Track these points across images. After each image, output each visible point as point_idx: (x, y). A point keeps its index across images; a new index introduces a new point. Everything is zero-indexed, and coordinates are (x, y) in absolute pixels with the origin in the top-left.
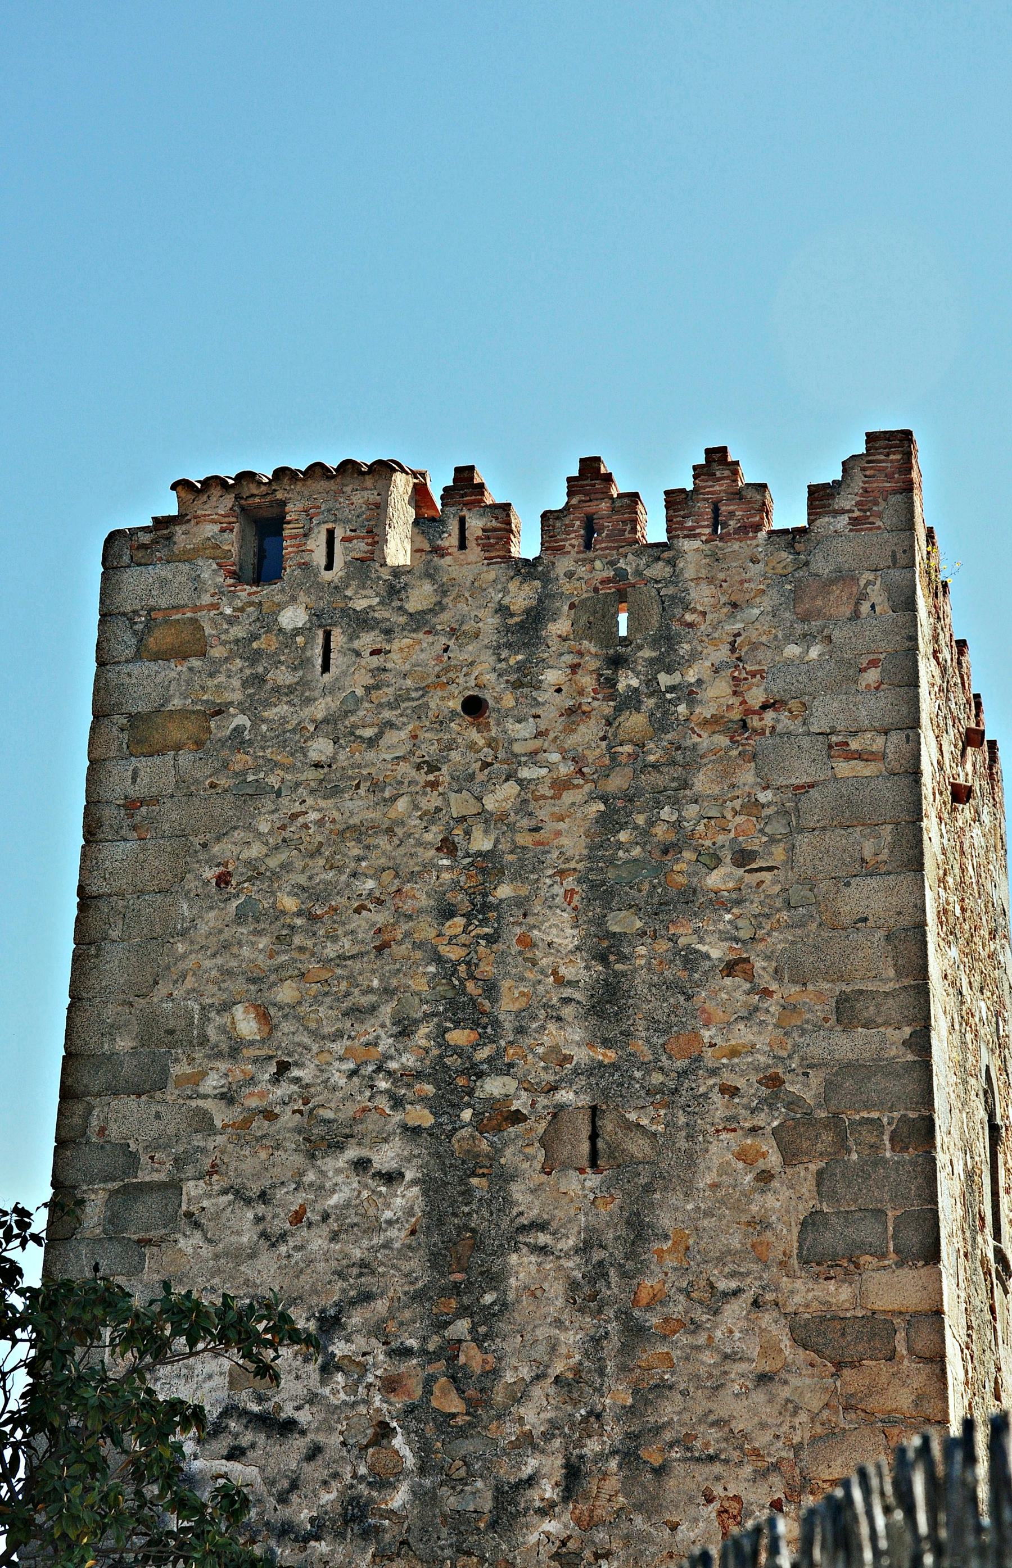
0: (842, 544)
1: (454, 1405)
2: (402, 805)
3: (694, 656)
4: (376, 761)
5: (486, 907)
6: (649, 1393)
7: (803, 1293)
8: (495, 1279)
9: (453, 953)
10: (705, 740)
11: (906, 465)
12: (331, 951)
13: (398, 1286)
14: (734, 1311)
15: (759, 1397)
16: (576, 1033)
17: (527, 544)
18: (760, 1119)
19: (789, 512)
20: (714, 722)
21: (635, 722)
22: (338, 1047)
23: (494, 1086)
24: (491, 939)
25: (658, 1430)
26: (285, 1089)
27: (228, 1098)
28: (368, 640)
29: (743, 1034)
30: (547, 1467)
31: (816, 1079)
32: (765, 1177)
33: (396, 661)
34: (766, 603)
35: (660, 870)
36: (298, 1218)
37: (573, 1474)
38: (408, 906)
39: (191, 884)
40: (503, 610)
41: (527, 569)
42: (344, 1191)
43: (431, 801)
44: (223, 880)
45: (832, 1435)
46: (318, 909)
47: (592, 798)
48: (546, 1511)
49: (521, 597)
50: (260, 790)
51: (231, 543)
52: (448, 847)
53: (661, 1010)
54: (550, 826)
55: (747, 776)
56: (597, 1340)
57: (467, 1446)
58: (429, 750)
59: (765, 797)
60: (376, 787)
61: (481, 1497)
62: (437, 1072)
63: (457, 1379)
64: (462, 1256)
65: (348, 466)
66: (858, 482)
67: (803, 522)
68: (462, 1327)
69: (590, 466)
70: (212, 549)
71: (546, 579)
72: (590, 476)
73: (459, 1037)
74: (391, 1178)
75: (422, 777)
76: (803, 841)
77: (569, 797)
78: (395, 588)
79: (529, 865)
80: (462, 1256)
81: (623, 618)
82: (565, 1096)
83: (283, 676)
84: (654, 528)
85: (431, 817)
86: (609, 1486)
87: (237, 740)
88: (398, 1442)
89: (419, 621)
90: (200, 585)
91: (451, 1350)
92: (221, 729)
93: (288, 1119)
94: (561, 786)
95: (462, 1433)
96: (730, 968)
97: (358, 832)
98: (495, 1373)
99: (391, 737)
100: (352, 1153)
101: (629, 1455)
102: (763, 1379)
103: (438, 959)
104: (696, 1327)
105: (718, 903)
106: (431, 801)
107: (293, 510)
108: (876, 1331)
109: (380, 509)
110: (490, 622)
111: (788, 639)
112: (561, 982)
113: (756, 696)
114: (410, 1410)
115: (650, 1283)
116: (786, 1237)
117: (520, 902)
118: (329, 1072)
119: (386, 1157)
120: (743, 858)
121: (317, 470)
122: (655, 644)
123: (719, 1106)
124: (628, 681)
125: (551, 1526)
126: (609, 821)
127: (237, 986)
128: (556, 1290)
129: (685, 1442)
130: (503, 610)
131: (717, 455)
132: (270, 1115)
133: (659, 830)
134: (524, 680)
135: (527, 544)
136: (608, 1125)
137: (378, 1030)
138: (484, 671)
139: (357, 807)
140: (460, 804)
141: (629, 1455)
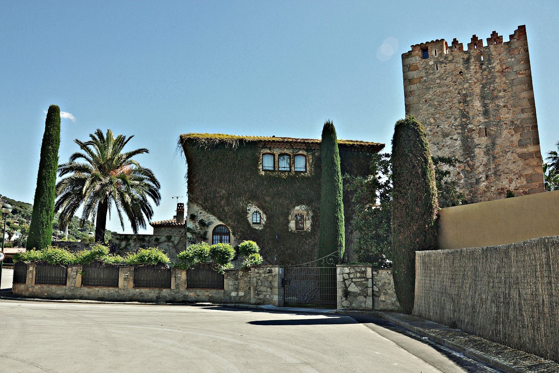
0: (516, 43)
1: (469, 169)
2: (451, 88)
3: (494, 62)
4: (447, 82)
5: (466, 101)
6: (497, 166)
7: (519, 150)
8: (473, 152)
9: (462, 108)
10: (497, 74)
11: (525, 30)
12: (443, 109)
13: (459, 154)
14: (509, 154)
15: (514, 165)
16: (482, 118)
17: (465, 48)
18: (511, 127)
19: (506, 39)
20: (498, 72)
21: (486, 73)
22: (446, 123)
23: (470, 126)
24: (467, 106)
25: (499, 170)
26: (439, 129)
27: (431, 131)
28: (443, 65)
29: (507, 116)
30: (483, 176)
31: (519, 121)
32: (512, 135)
33: (448, 68)
34: (504, 53)
35: (492, 93)
36: (443, 146)
37: (487, 177)
38: (454, 102)
39: (421, 102)
40: (463, 59)
41: (466, 52)
42: (449, 142)
43: (456, 87)
44: (426, 101)
45: (525, 169)
46: (440, 104)
47: (480, 84)
48: (484, 181)
49: (466, 56)
50: (430, 88)
51: (420, 53)
52: (459, 93)
53: (494, 114)
54: (474, 89)
55: (504, 79)
56: (489, 159)
57: (471, 174)
58: (454, 80)
59: (507, 81)
60: (447, 86)
61: (474, 180)
62: (461, 125)
63: (469, 166)
64: (468, 149)
65: (437, 41)
66: (517, 34)
67: (509, 40)
68: (469, 159)
69: (474, 36)
70: (418, 55)
71: (469, 53)
72: (474, 38)
73: (464, 120)
74: (456, 140)
75: (454, 84)
76: (514, 87)
77: (477, 84)
78: (446, 58)
79: (472, 95)
80: (468, 149)
81: (482, 58)
82: (481, 127)
83: (431, 71)
84: (485, 44)
85: (456, 89)
86: (493, 178)
87: (425, 81)
88: (461, 174)
89: (451, 61)
90: (416, 59)
91: (467, 162)
92: (423, 80)
93: (440, 133)
94: (475, 83)
95: (470, 172)
96: (504, 106)
97: (445, 92)
98: (474, 164)
99: (448, 78)
100: (450, 137)
101: (495, 174)
102: (514, 162)
103: (460, 109)
104: (504, 156)
105: (501, 98)
106: (456, 87)
107: (429, 48)
108: (531, 155)
109: (443, 46)
110: (462, 60)
111: (509, 58)
112: (478, 111)
113: (504, 67)
114: (462, 170)
115: (496, 151)
116: (516, 143)
117: (471, 100)
118: (445, 126)
119: (455, 137)
120: (505, 91)
121: (432, 41)
122: (488, 61)
123: (504, 126)
124: (484, 67)
125: (484, 183)
126: (483, 87)
127: (430, 115)
128: (482, 153)
129: (503, 171)
130: (463, 59)
131: (494, 32)
132: (437, 133)
133: (491, 88)
134: (468, 68)
135: (465, 48)
136: (488, 130)
137: (452, 120)
138: (461, 67)
139: (445, 89)
140: (460, 87)
141: (495, 174)
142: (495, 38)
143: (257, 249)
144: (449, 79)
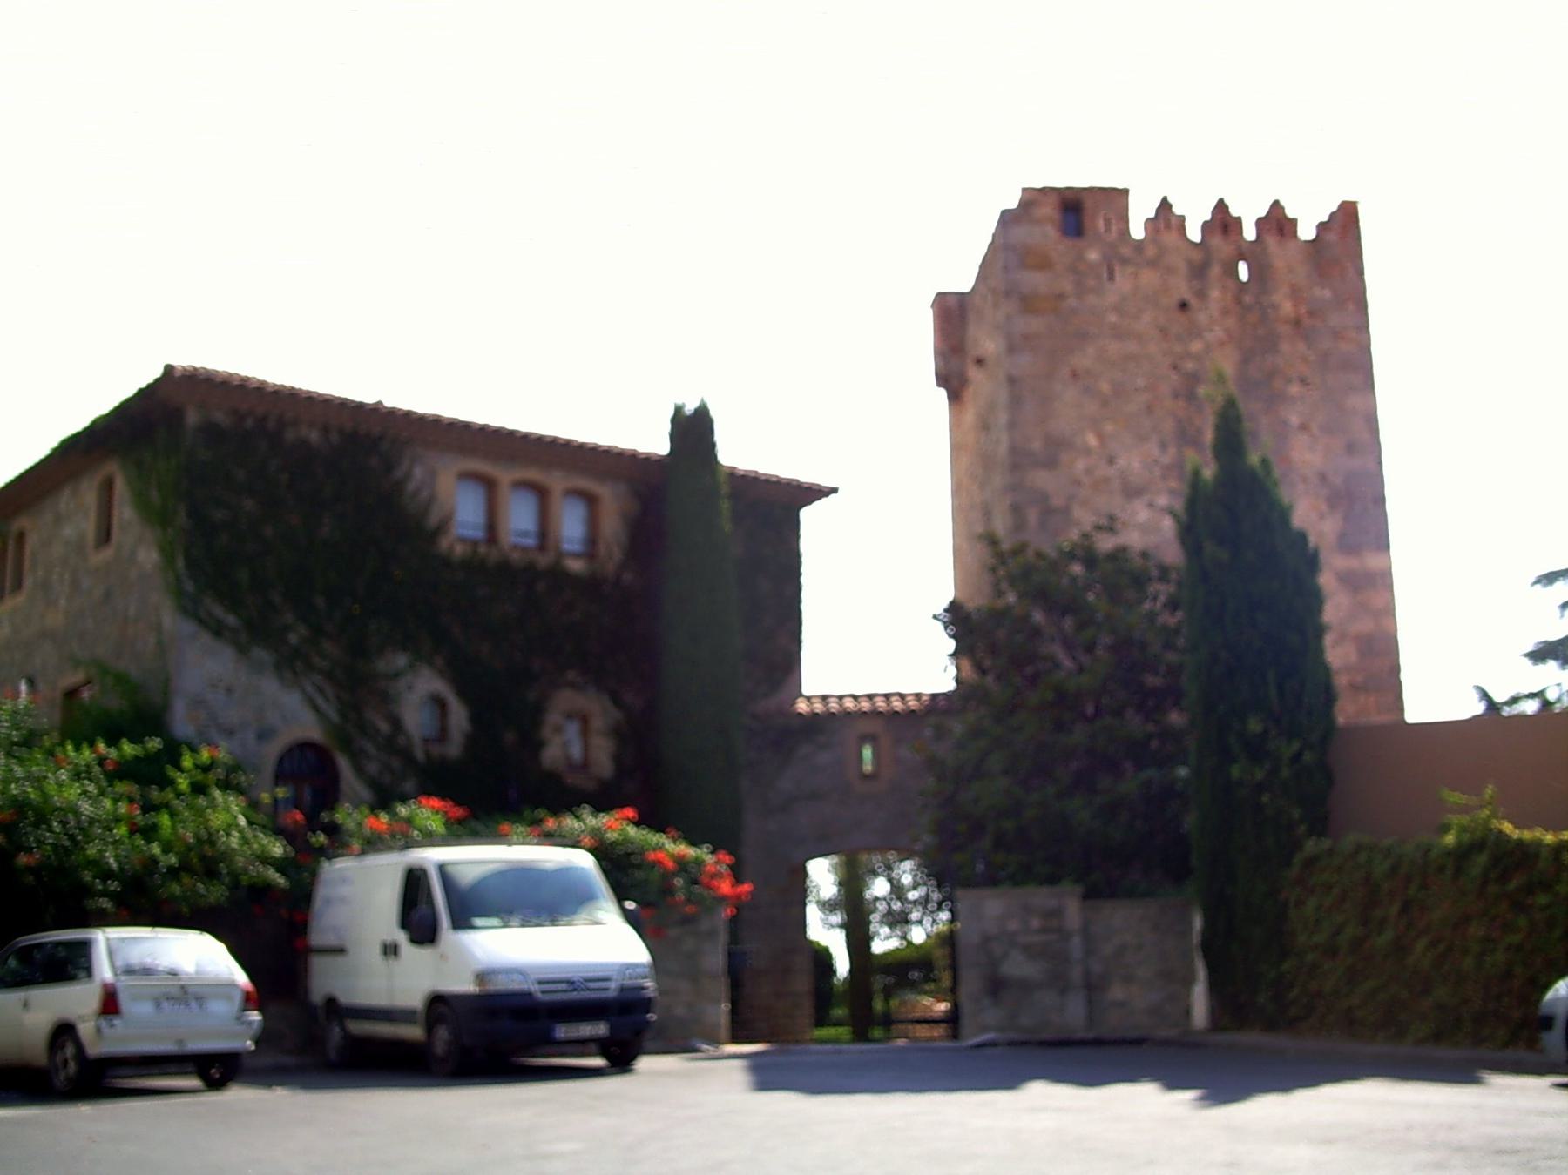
26: (1111, 472)
28: (1130, 269)
81: (867, 753)
134: (1201, 295)
138: (1182, 288)
139: (1132, 347)
140: (1178, 348)
142: (1277, 222)
143: (813, 913)
144: (1147, 318)
